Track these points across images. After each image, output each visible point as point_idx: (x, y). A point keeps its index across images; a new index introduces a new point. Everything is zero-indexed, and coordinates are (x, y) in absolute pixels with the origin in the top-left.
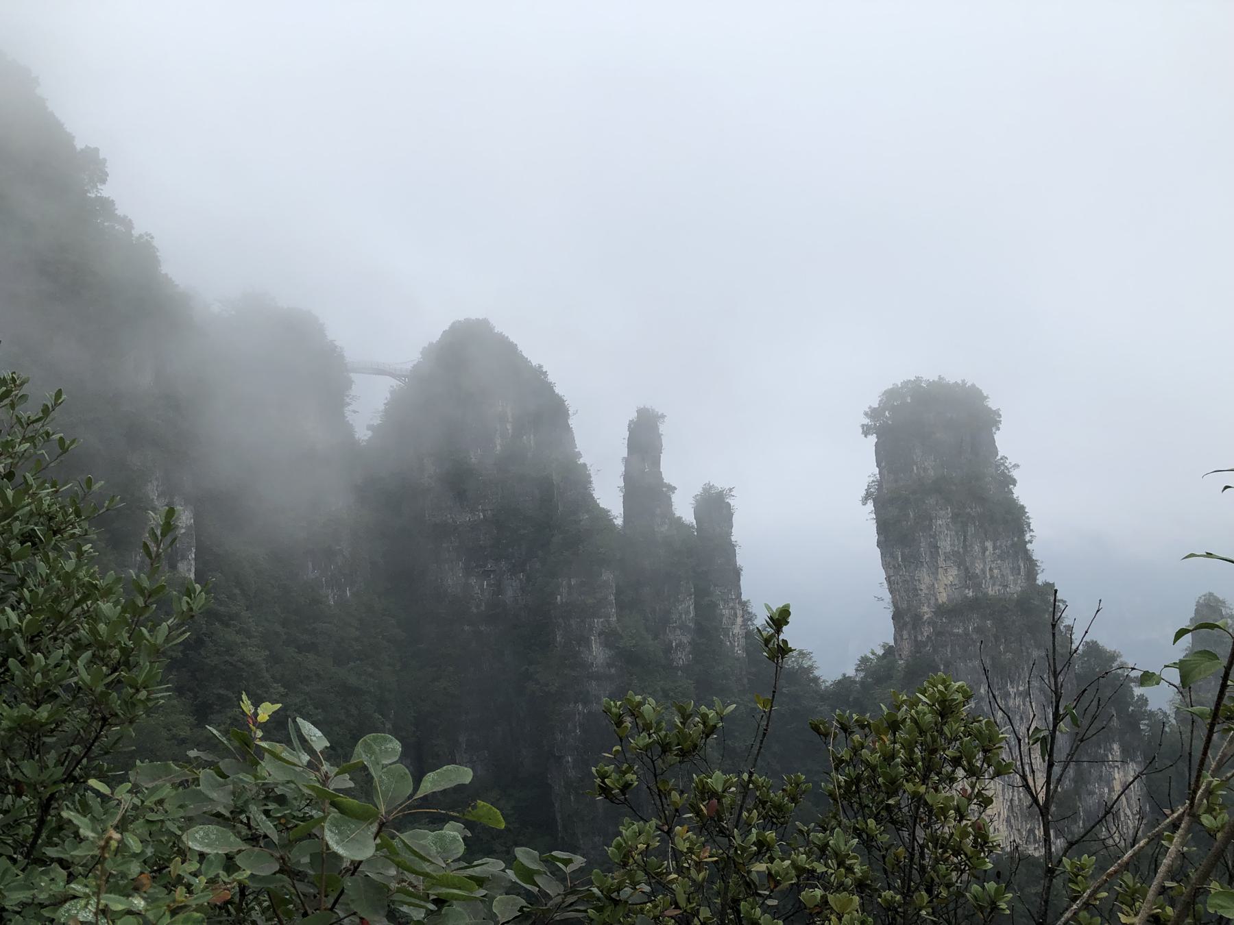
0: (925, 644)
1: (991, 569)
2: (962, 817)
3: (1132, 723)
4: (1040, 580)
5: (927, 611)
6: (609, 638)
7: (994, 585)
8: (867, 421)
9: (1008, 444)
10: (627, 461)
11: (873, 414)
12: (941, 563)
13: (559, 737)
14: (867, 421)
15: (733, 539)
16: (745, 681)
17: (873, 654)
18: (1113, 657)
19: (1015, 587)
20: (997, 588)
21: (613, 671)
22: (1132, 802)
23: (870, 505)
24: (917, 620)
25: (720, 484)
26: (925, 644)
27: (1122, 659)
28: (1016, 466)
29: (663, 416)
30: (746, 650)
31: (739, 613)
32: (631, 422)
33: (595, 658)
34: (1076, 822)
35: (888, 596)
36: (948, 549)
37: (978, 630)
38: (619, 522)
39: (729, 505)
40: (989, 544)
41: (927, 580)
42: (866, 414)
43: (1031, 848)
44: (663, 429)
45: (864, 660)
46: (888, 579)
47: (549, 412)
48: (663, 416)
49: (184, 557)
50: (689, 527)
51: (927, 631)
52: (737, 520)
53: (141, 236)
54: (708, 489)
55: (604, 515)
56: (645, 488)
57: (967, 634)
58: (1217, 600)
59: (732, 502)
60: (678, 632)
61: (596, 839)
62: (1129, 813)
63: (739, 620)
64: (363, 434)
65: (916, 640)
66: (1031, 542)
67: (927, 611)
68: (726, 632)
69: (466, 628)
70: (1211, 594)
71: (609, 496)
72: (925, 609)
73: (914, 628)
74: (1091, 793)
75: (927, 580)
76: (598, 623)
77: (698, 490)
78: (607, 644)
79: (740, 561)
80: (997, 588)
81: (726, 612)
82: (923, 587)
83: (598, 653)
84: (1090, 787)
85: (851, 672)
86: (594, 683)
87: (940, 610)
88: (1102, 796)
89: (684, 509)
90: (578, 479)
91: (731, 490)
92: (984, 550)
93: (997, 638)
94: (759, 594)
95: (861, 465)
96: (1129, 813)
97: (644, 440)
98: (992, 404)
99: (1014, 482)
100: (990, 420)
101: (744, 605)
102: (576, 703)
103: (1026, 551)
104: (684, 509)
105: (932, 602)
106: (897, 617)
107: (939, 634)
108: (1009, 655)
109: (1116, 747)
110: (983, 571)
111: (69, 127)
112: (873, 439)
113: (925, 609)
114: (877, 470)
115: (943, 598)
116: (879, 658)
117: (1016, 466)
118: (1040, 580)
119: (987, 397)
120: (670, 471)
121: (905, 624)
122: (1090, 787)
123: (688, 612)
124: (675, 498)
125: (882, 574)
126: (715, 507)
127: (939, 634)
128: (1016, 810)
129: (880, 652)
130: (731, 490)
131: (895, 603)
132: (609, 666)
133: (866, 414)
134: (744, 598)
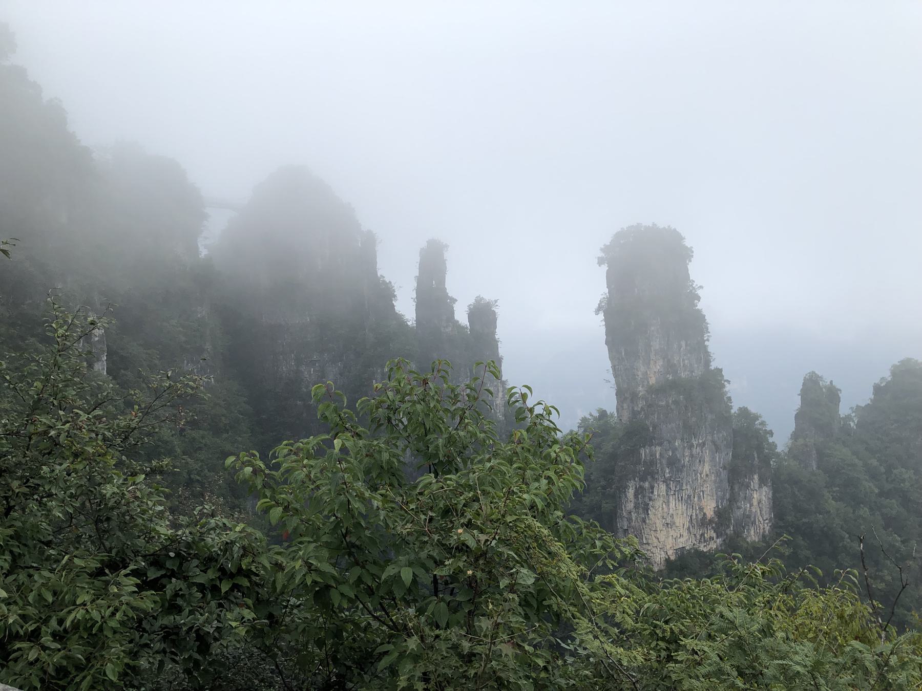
0: (639, 413)
1: (683, 360)
3: (765, 460)
4: (713, 366)
5: (641, 390)
7: (685, 371)
8: (601, 255)
9: (697, 272)
11: (605, 249)
12: (652, 357)
14: (601, 255)
15: (497, 337)
17: (591, 415)
18: (756, 417)
19: (698, 372)
20: (687, 373)
22: (763, 512)
23: (601, 316)
24: (634, 397)
25: (488, 297)
26: (639, 413)
27: (763, 419)
28: (701, 287)
29: (447, 246)
30: (505, 415)
31: (501, 389)
34: (729, 527)
35: (613, 380)
36: (657, 347)
37: (676, 402)
39: (494, 312)
40: (683, 343)
41: (643, 369)
42: (601, 249)
43: (702, 545)
44: (447, 255)
45: (584, 420)
46: (614, 367)
47: (369, 246)
48: (447, 246)
49: (98, 360)
50: (464, 328)
51: (641, 404)
52: (499, 323)
53: (817, 398)
54: (479, 300)
55: (399, 318)
56: (432, 297)
57: (668, 406)
58: (817, 376)
59: (496, 311)
62: (761, 519)
64: (204, 253)
65: (633, 408)
66: (708, 340)
67: (641, 390)
69: (299, 403)
70: (813, 372)
71: (406, 307)
72: (640, 388)
73: (632, 401)
74: (739, 508)
75: (643, 369)
77: (472, 301)
79: (501, 351)
80: (687, 373)
82: (639, 373)
84: (739, 504)
85: (576, 429)
87: (651, 390)
88: (745, 510)
89: (461, 316)
90: (386, 294)
91: (496, 301)
92: (680, 347)
93: (686, 407)
94: (514, 374)
95: (595, 287)
96: (761, 519)
98: (688, 243)
99: (699, 298)
100: (685, 255)
103: (706, 347)
104: (461, 316)
105: (646, 383)
106: (620, 393)
107: (650, 406)
108: (694, 419)
109: (756, 477)
110: (679, 361)
112: (605, 268)
113: (640, 388)
114: (607, 291)
115: (652, 381)
116: (595, 419)
117: (701, 287)
118: (713, 366)
119: (654, 224)
120: (452, 288)
121: (626, 399)
122: (739, 504)
124: (456, 307)
125: (609, 364)
126: (483, 314)
127: (650, 406)
128: (694, 522)
129: (596, 414)
130: (496, 301)
131: (617, 383)
133: (601, 249)
134: (503, 379)
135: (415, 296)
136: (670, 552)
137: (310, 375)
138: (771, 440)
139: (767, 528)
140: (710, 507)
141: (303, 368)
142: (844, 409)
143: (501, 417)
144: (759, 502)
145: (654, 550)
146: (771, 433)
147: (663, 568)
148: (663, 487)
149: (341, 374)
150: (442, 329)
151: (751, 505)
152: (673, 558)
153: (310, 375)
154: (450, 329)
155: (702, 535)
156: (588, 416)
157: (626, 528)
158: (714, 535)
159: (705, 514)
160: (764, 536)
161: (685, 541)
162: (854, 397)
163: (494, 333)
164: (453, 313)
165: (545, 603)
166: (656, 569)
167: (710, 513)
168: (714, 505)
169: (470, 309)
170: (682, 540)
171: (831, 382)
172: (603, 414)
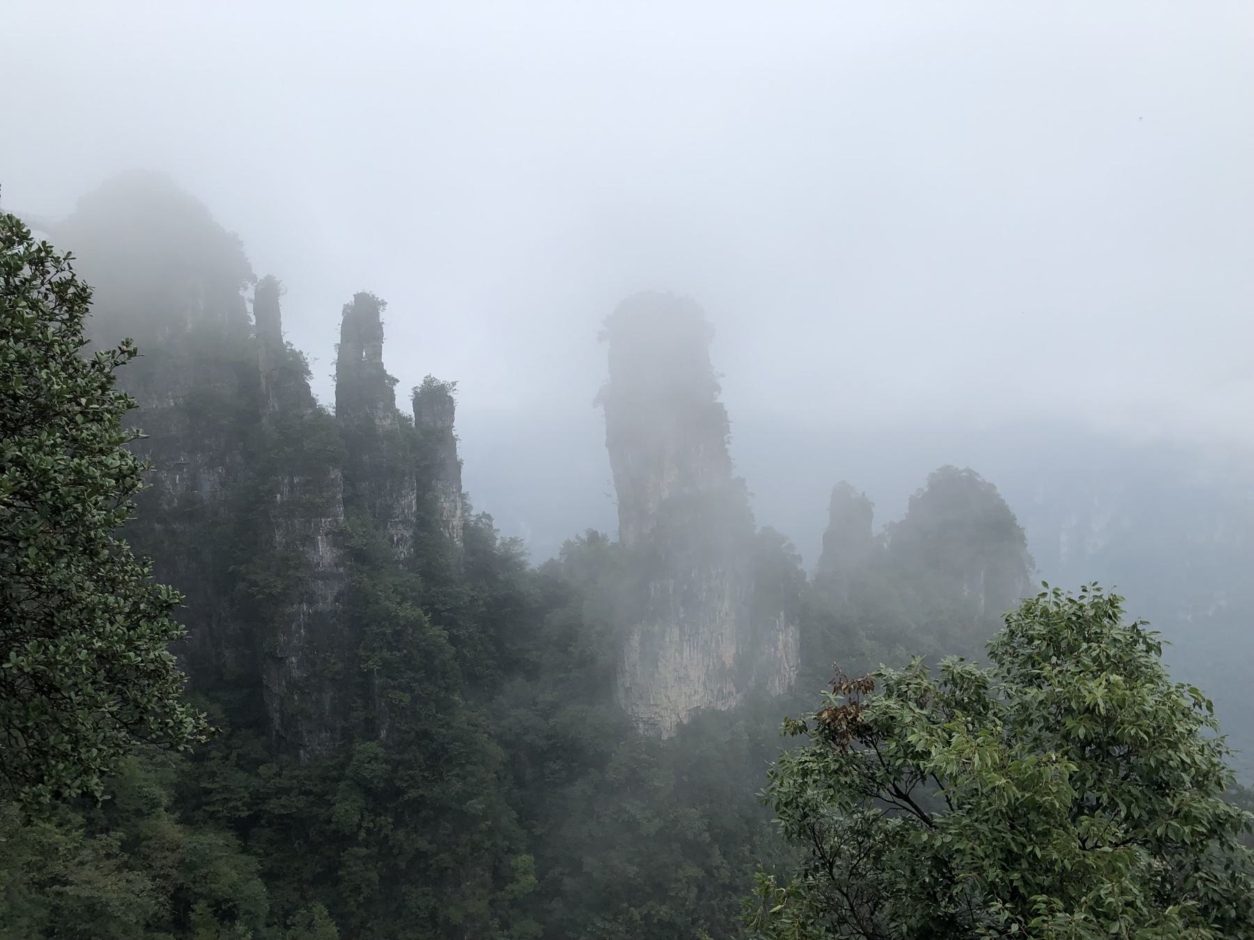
2: (376, 758)
6: (338, 537)
10: (341, 348)
13: (282, 638)
15: (454, 433)
16: (462, 570)
17: (577, 537)
21: (341, 570)
25: (442, 377)
28: (723, 375)
29: (384, 303)
31: (459, 505)
32: (346, 307)
33: (322, 557)
38: (333, 414)
44: (384, 316)
45: (568, 544)
48: (384, 303)
54: (429, 382)
59: (454, 397)
60: (400, 526)
61: (324, 735)
63: (459, 513)
68: (446, 524)
69: (157, 526)
71: (323, 390)
76: (326, 522)
77: (419, 382)
78: (335, 544)
81: (446, 505)
83: (325, 553)
85: (557, 557)
86: (320, 582)
89: (404, 404)
91: (454, 384)
97: (362, 327)
99: (719, 389)
101: (463, 497)
102: (300, 603)
104: (404, 404)
109: (782, 614)
111: (263, 261)
117: (723, 375)
120: (391, 361)
123: (410, 507)
124: (397, 389)
126: (435, 398)
129: (584, 537)
130: (454, 384)
132: (337, 565)
134: (463, 491)
135: (334, 372)
136: (682, 714)
137: (174, 484)
138: (800, 567)
139: (794, 677)
140: (728, 653)
141: (163, 475)
142: (877, 528)
143: (459, 544)
144: (785, 645)
145: (663, 713)
146: (799, 558)
147: (673, 735)
148: (676, 631)
149: (222, 484)
150: (377, 421)
151: (776, 649)
152: (685, 721)
153: (174, 484)
154: (389, 421)
155: (721, 690)
156: (573, 539)
157: (628, 685)
158: (734, 690)
159: (724, 663)
160: (790, 688)
161: (700, 699)
162: (890, 510)
163: (450, 427)
164: (393, 398)
165: (389, 767)
166: (665, 737)
167: (729, 661)
168: (733, 651)
169: (416, 393)
170: (697, 697)
171: (362, 327)
172: (594, 538)
